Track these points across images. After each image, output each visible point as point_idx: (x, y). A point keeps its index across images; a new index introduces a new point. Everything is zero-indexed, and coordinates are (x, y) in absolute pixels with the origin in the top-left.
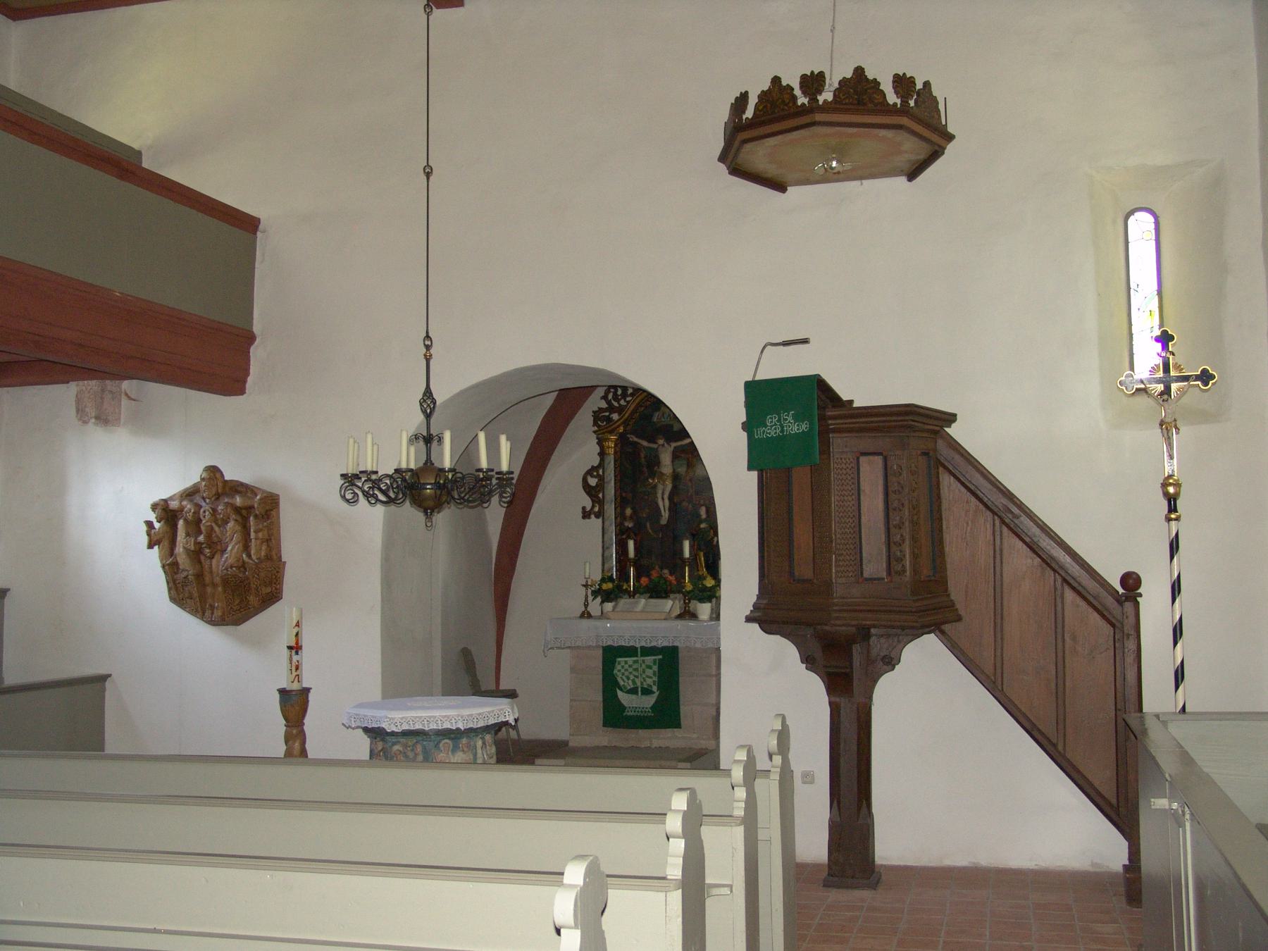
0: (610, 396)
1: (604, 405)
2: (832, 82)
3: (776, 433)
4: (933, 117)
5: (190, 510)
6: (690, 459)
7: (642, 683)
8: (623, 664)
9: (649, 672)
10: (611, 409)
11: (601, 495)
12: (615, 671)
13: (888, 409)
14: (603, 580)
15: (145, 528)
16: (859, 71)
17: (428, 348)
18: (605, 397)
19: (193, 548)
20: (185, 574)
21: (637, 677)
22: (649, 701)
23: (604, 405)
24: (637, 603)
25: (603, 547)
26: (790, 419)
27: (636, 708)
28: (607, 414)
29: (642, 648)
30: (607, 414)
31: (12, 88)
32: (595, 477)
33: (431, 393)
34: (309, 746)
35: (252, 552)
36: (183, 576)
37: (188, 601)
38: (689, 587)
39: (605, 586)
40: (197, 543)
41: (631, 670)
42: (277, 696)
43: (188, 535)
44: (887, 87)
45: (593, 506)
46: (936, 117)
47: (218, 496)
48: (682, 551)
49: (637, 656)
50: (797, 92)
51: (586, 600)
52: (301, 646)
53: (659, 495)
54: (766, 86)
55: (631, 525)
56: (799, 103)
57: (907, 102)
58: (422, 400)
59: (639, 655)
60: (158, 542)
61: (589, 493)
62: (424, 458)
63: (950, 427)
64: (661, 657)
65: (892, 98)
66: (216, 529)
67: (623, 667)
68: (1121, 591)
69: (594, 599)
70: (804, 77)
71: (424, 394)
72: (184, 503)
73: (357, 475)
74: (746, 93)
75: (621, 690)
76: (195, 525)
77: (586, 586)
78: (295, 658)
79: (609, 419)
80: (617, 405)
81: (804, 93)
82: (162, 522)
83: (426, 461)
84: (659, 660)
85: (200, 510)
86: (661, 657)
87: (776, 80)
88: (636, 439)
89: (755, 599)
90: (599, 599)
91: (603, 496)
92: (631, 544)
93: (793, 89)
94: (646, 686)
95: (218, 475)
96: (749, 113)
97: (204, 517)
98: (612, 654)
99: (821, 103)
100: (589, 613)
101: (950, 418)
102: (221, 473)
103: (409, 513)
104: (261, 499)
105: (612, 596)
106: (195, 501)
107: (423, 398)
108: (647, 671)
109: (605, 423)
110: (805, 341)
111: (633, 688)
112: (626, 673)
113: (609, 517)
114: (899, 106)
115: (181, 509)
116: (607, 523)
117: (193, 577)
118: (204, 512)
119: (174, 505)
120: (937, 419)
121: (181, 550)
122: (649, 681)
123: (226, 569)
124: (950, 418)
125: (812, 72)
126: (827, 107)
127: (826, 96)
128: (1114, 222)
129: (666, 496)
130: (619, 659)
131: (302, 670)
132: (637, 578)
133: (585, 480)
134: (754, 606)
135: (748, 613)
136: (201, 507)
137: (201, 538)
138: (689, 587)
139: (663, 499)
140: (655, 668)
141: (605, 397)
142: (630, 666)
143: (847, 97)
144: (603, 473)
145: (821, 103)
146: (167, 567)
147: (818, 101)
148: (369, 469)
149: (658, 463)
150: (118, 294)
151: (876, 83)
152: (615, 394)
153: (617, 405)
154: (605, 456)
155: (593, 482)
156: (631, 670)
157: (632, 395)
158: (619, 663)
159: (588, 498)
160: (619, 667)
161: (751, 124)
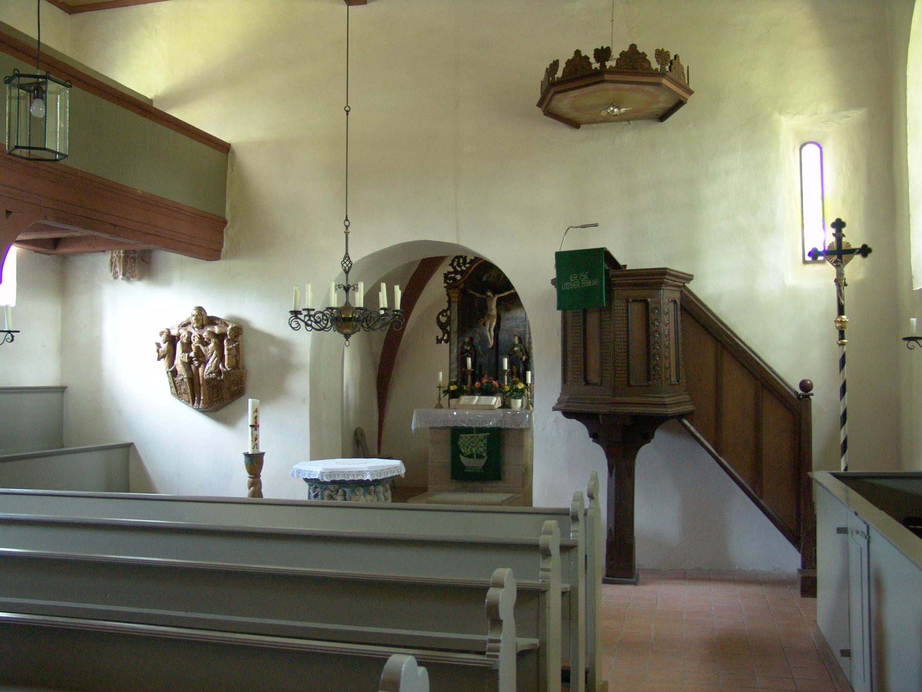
0: (455, 264)
1: (451, 270)
2: (616, 54)
3: (576, 286)
4: (680, 78)
5: (185, 336)
7: (476, 451)
8: (464, 438)
9: (481, 444)
10: (456, 272)
12: (459, 443)
13: (660, 270)
14: (451, 384)
15: (156, 347)
16: (633, 47)
17: (347, 227)
18: (452, 265)
19: (186, 361)
20: (182, 377)
21: (473, 447)
22: (482, 462)
23: (451, 270)
24: (473, 399)
25: (450, 362)
26: (585, 277)
27: (472, 467)
28: (453, 275)
29: (477, 428)
30: (453, 275)
31: (68, 55)
32: (445, 316)
33: (349, 258)
34: (263, 490)
35: (226, 364)
36: (180, 379)
37: (183, 395)
38: (507, 388)
39: (452, 388)
40: (190, 358)
41: (469, 442)
42: (243, 457)
43: (183, 352)
44: (651, 57)
46: (682, 78)
47: (202, 327)
48: (502, 365)
50: (592, 60)
51: (440, 396)
52: (259, 425)
54: (571, 56)
55: (468, 348)
56: (593, 67)
57: (664, 68)
58: (343, 262)
60: (164, 357)
62: (344, 300)
63: (689, 283)
64: (489, 434)
65: (655, 65)
66: (202, 348)
67: (464, 440)
68: (800, 392)
69: (444, 396)
70: (596, 51)
71: (345, 258)
72: (181, 331)
73: (301, 312)
74: (558, 61)
75: (463, 455)
76: (187, 347)
77: (440, 387)
78: (255, 432)
79: (454, 279)
81: (597, 61)
82: (167, 343)
83: (346, 302)
84: (488, 436)
85: (191, 335)
86: (489, 434)
87: (578, 52)
88: (471, 292)
89: (558, 396)
90: (447, 396)
92: (469, 360)
93: (589, 58)
94: (479, 453)
95: (203, 313)
96: (559, 74)
97: (194, 340)
98: (457, 432)
99: (608, 67)
100: (441, 405)
101: (689, 278)
102: (205, 311)
103: (333, 336)
104: (231, 329)
106: (188, 330)
107: (344, 261)
108: (480, 445)
109: (451, 281)
110: (596, 225)
111: (471, 454)
112: (466, 444)
114: (659, 70)
115: (179, 335)
117: (187, 380)
118: (194, 337)
119: (174, 332)
120: (683, 278)
121: (179, 362)
122: (481, 450)
123: (209, 374)
124: (689, 278)
125: (602, 47)
126: (612, 71)
127: (611, 64)
128: (794, 149)
129: (492, 330)
130: (462, 435)
131: (259, 440)
132: (473, 383)
133: (438, 318)
134: (558, 400)
135: (554, 405)
136: (192, 334)
137: (192, 354)
138: (507, 388)
139: (490, 331)
140: (485, 441)
141: (452, 265)
142: (469, 440)
143: (625, 64)
144: (450, 314)
145: (608, 67)
146: (169, 373)
147: (606, 66)
148: (310, 307)
150: (140, 192)
151: (644, 55)
152: (458, 262)
153: (460, 270)
155: (443, 319)
156: (469, 442)
157: (469, 263)
158: (462, 438)
159: (440, 330)
160: (461, 440)
161: (561, 82)
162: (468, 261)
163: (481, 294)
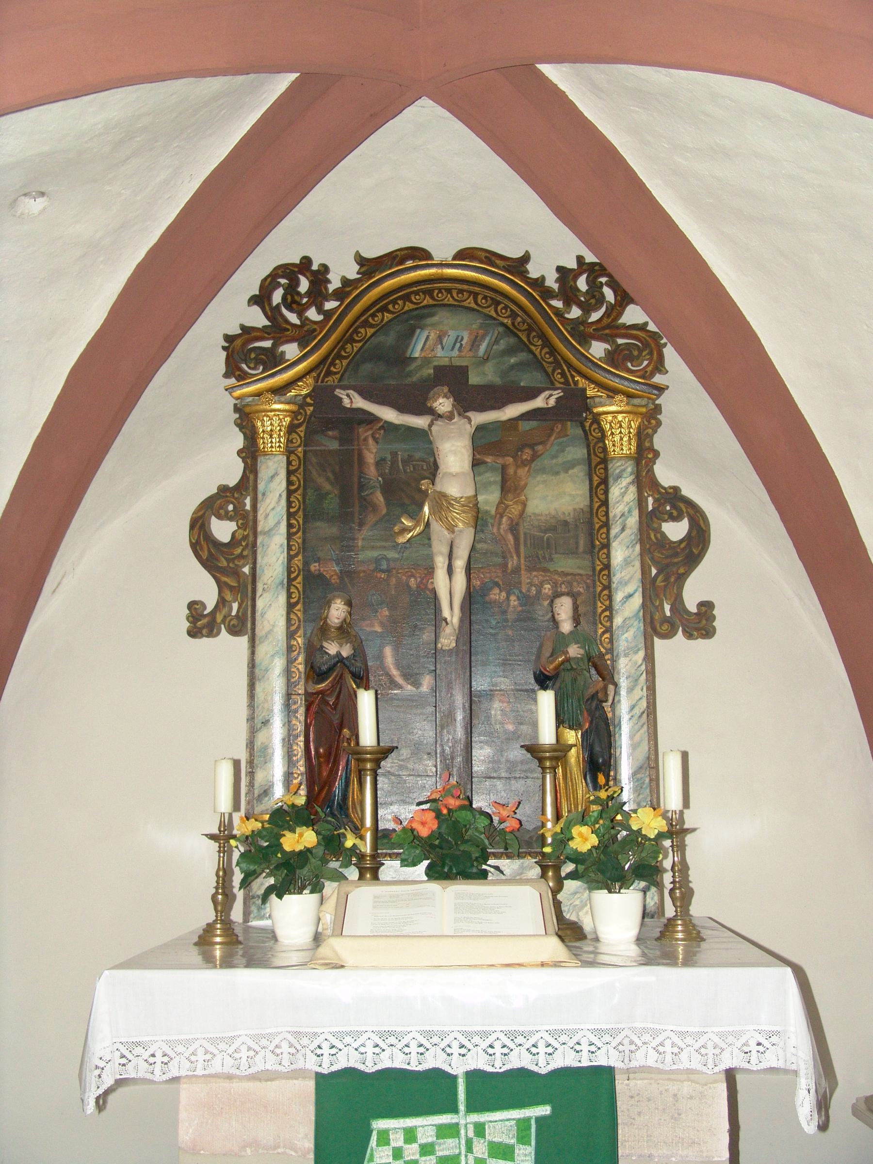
0: (277, 297)
1: (257, 318)
6: (511, 471)
8: (397, 1140)
11: (246, 570)
23: (257, 318)
25: (251, 719)
28: (267, 344)
29: (475, 1076)
30: (267, 344)
45: (222, 602)
49: (455, 1110)
53: (441, 562)
59: (462, 1107)
61: (209, 564)
64: (545, 1110)
80: (298, 322)
84: (539, 1120)
86: (545, 1110)
88: (360, 403)
91: (254, 570)
105: (305, 872)
113: (270, 632)
116: (263, 650)
141: (260, 300)
149: (433, 470)
152: (292, 289)
153: (298, 322)
154: (261, 459)
157: (339, 295)
158: (384, 1137)
162: (335, 283)
163: (402, 409)
